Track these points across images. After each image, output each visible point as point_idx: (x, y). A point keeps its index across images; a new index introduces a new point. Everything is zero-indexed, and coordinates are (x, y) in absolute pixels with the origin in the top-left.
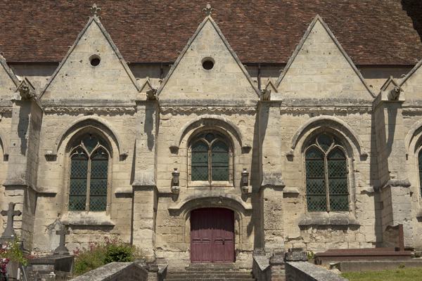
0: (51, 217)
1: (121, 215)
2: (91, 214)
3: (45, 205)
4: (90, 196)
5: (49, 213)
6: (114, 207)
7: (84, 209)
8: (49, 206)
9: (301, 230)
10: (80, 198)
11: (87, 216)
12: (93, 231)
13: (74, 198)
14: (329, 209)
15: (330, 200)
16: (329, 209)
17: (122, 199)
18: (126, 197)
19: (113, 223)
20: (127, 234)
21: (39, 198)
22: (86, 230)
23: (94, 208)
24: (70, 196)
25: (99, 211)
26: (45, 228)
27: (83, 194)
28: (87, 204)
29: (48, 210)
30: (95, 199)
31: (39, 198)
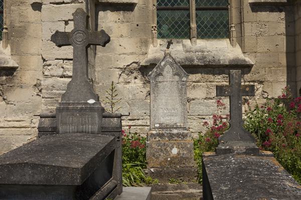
0: (129, 51)
1: (263, 46)
2: (201, 43)
3: (114, 27)
4: (197, 9)
5: (124, 42)
6: (249, 29)
7: (188, 36)
8: (124, 29)
9: (143, 74)
10: (178, 14)
11: (194, 47)
12: (211, 77)
13: (166, 13)
14: (194, 32)
15: (197, 15)
16: (194, 32)
17: (264, 15)
18: (272, 11)
19: (249, 60)
20: (278, 82)
21: (101, 14)
22: (199, 75)
23: (204, 34)
24: (158, 10)
25: (215, 37)
26: (118, 72)
27: (182, 5)
28: (193, 25)
29: (122, 36)
30: (207, 16)
31: (101, 14)
